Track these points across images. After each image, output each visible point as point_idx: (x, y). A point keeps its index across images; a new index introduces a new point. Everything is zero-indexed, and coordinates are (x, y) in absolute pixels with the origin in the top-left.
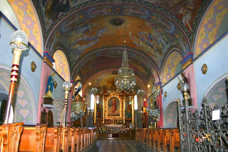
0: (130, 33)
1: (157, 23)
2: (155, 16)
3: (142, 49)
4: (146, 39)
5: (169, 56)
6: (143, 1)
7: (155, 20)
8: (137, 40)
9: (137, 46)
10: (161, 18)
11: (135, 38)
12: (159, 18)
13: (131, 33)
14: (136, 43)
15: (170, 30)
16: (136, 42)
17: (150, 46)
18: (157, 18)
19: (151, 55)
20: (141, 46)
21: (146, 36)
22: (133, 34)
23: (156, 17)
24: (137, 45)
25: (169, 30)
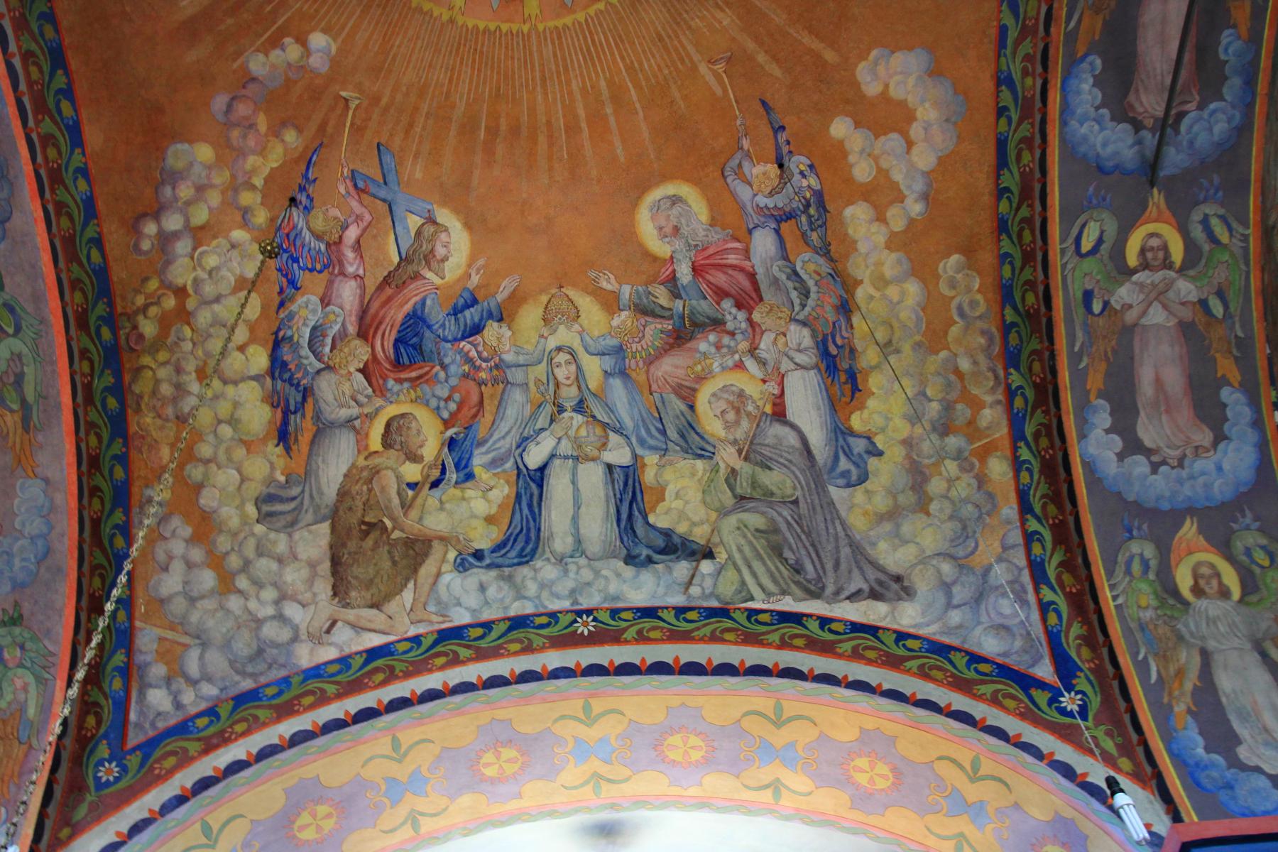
0: (318, 40)
1: (1088, 296)
2: (1198, 233)
3: (148, 328)
4: (348, 293)
5: (1042, 767)
6: (84, 172)
7: (1132, 259)
8: (234, 188)
9: (150, 228)
10: (1203, 303)
11: (262, 151)
12: (1186, 289)
13: (318, 62)
14: (185, 191)
15: (1155, 468)
16: (200, 189)
17: (274, 400)
18: (1167, 264)
19: (161, 493)
20: (181, 292)
21: (394, 281)
22: (315, 94)
23: (1190, 245)
24: (173, 222)
25: (1133, 446)
